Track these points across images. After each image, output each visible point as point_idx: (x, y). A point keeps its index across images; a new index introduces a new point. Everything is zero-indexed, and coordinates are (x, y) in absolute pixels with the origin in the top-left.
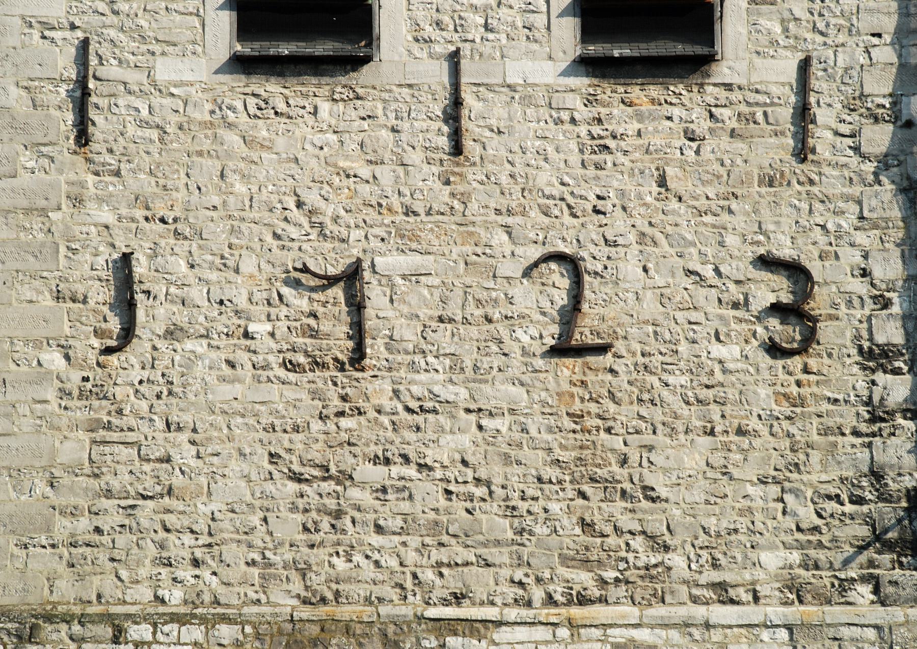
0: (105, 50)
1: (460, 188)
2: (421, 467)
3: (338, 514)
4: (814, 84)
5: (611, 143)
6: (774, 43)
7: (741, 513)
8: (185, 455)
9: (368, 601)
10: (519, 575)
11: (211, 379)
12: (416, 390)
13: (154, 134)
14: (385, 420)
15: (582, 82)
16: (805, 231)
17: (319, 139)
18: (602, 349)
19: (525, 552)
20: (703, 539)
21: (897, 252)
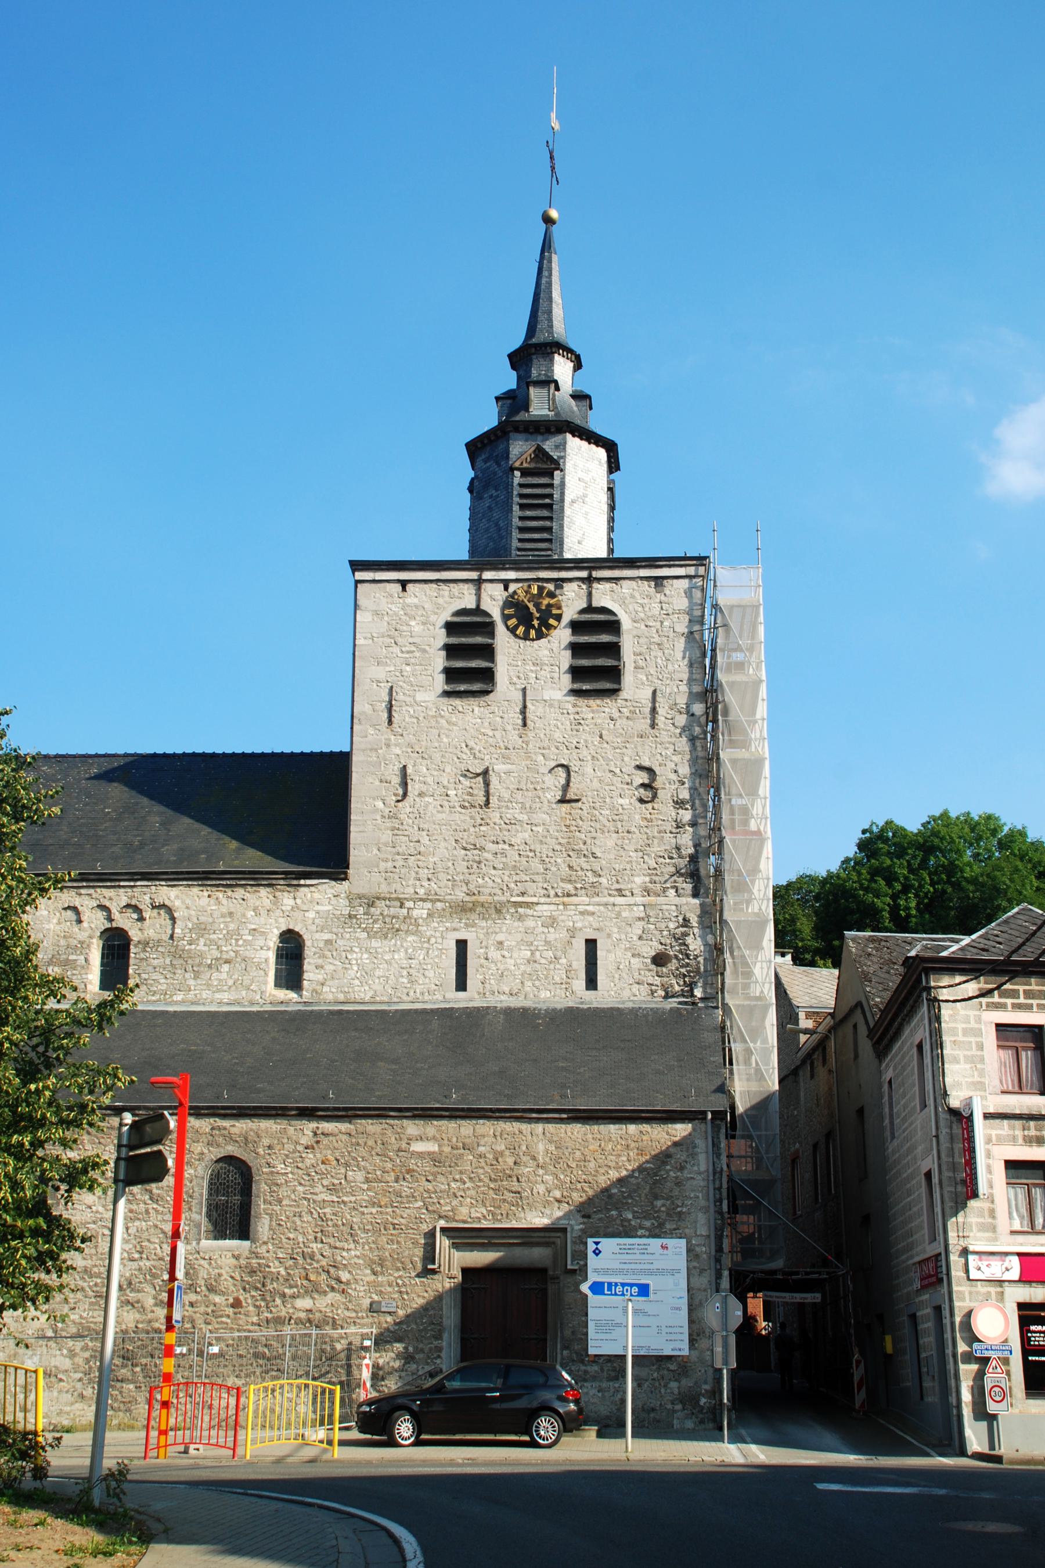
0: (398, 690)
1: (526, 739)
2: (510, 845)
3: (480, 862)
4: (658, 699)
5: (582, 722)
6: (643, 684)
7: (628, 863)
8: (425, 840)
9: (490, 895)
10: (545, 886)
11: (434, 812)
12: (508, 816)
13: (415, 721)
14: (497, 827)
15: (572, 699)
16: (654, 755)
17: (474, 721)
18: (577, 801)
19: (548, 877)
20: (613, 872)
21: (687, 764)
